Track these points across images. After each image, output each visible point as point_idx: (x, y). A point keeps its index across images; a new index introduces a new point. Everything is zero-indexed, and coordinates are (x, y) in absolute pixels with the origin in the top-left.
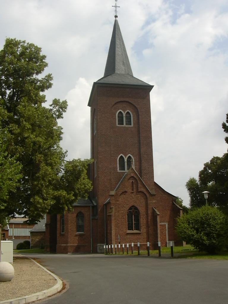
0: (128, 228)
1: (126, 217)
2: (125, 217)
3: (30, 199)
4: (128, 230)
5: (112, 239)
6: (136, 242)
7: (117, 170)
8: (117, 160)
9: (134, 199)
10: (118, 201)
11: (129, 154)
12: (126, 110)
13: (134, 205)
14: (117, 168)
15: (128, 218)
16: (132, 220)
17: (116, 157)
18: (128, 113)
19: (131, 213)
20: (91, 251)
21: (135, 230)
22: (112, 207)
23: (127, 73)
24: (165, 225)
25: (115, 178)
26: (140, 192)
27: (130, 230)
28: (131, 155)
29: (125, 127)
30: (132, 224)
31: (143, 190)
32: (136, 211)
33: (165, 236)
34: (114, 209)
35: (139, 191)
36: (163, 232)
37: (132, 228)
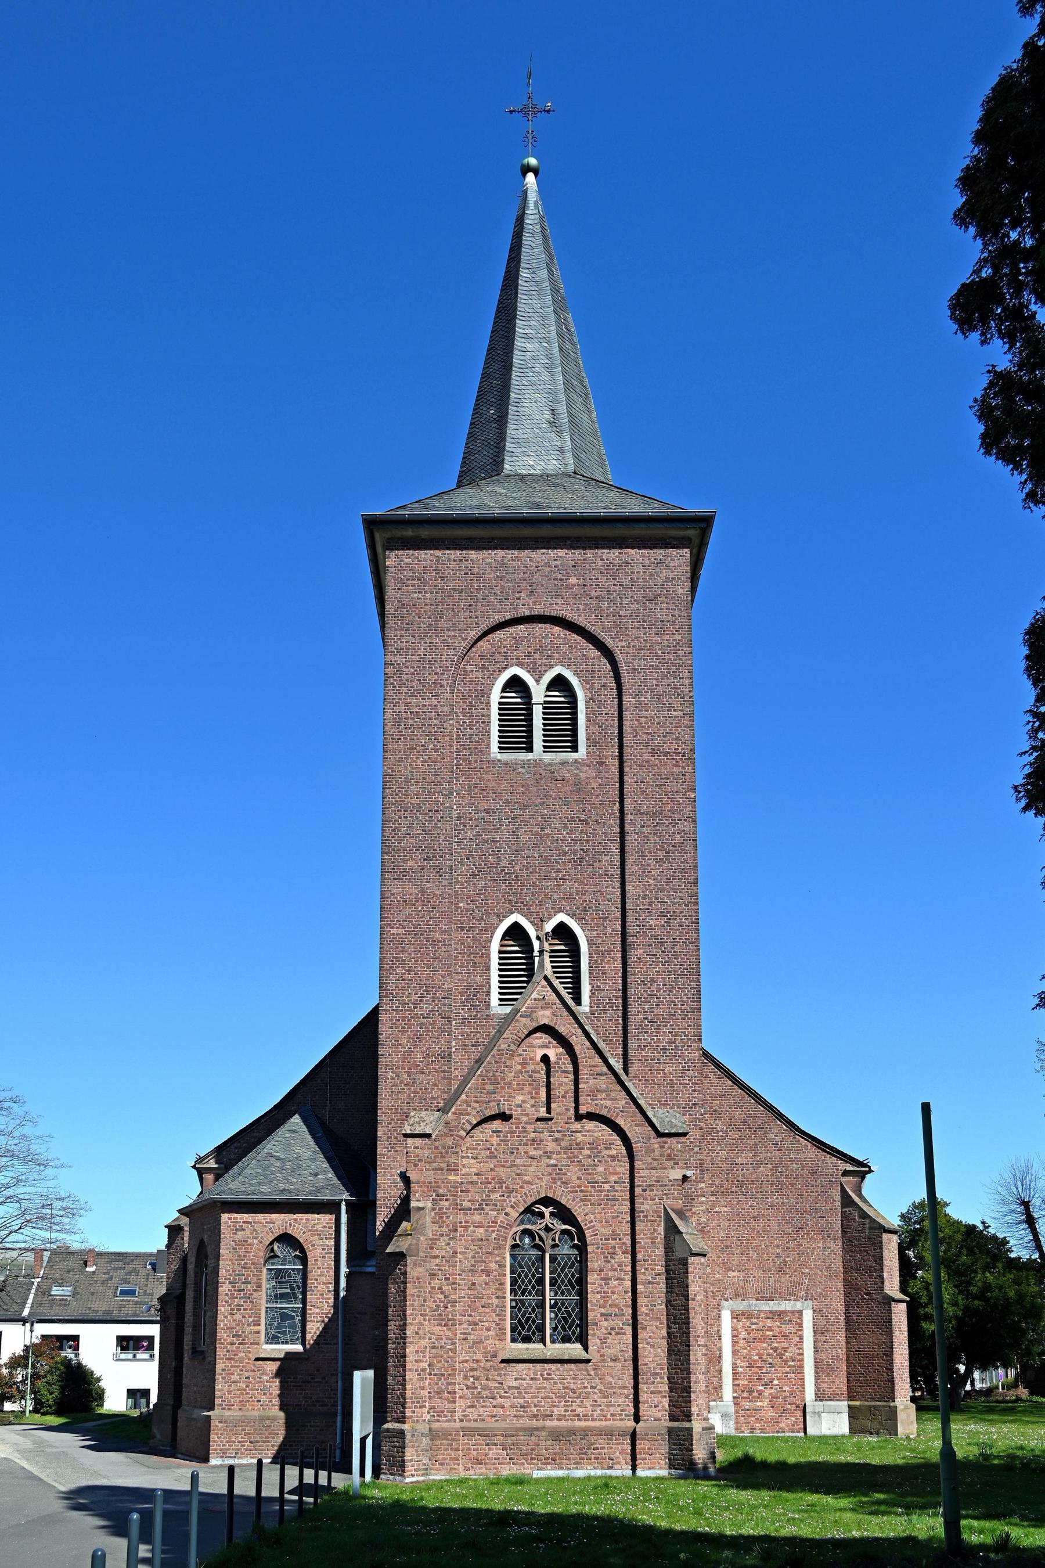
0: (513, 1330)
1: (502, 1266)
2: (494, 1266)
3: (920, 1270)
4: (513, 1340)
5: (408, 1393)
6: (556, 1411)
7: (488, 1006)
8: (488, 949)
9: (553, 1162)
10: (452, 1169)
11: (560, 911)
12: (552, 667)
13: (550, 1195)
14: (488, 993)
15: (512, 1272)
16: (541, 1281)
17: (481, 932)
18: (559, 683)
19: (537, 1241)
20: (338, 1452)
21: (553, 1341)
22: (420, 1204)
23: (571, 468)
24: (800, 1312)
25: (831, 1163)
26: (591, 1116)
27: (527, 1340)
28: (572, 915)
29: (537, 763)
30: (542, 1305)
31: (615, 1105)
32: (567, 1227)
33: (800, 1371)
34: (428, 1220)
35: (583, 1110)
36: (785, 1350)
37: (541, 1329)
